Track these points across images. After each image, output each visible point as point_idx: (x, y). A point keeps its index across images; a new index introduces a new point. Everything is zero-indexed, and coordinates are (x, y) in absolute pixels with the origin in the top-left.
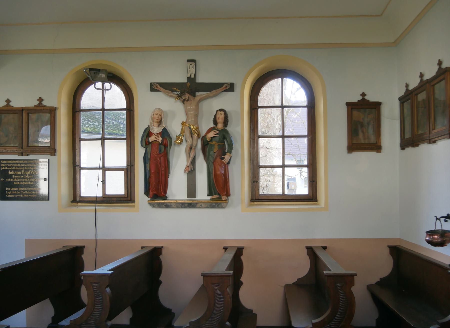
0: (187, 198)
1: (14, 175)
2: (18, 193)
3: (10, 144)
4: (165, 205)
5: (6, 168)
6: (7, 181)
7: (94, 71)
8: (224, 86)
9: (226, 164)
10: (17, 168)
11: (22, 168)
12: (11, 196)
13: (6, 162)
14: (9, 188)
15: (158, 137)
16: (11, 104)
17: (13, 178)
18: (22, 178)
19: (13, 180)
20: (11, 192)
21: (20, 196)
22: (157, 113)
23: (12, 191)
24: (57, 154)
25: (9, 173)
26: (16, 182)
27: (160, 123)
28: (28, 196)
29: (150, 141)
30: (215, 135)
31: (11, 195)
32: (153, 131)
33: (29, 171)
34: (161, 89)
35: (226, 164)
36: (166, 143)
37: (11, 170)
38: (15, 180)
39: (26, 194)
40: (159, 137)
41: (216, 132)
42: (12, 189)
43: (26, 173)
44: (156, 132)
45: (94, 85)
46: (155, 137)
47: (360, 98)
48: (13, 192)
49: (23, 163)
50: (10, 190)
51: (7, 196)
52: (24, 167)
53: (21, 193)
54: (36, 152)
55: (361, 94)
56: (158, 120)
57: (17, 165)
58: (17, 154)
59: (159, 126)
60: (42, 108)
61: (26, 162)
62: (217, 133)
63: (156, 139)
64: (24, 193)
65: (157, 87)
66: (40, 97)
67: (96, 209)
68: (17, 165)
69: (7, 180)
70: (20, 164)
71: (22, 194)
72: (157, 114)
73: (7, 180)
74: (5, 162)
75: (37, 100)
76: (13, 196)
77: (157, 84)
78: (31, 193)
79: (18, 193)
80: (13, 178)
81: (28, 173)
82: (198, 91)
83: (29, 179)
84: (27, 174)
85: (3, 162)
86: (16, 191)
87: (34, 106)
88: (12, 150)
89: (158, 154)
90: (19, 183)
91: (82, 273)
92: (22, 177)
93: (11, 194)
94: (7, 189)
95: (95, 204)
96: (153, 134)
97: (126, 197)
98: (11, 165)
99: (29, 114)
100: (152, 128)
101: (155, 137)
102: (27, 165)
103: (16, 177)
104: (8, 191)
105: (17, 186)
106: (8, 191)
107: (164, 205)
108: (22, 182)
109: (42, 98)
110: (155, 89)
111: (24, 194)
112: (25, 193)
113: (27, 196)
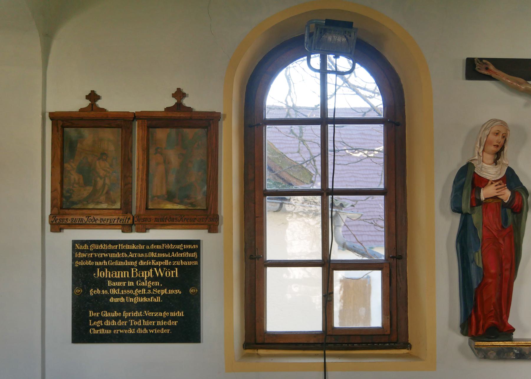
1: (110, 279)
2: (120, 323)
3: (98, 203)
4: (514, 353)
5: (90, 263)
6: (91, 294)
10: (117, 263)
11: (131, 263)
12: (102, 331)
13: (89, 248)
14: (96, 312)
16: (100, 104)
17: (108, 288)
18: (131, 288)
19: (109, 292)
20: (103, 323)
21: (126, 331)
22: (497, 132)
23: (104, 319)
24: (222, 227)
25: (96, 275)
26: (115, 296)
27: (498, 155)
28: (148, 331)
29: (483, 198)
31: (103, 330)
32: (484, 173)
33: (151, 270)
34: (500, 74)
36: (520, 203)
37: (102, 268)
38: (114, 291)
39: (142, 327)
40: (505, 189)
42: (106, 314)
43: (141, 275)
44: (493, 177)
45: (306, 58)
46: (497, 189)
47: (172, 102)
48: (108, 323)
49: (134, 251)
50: (101, 318)
51: (92, 331)
52: (139, 259)
53: (129, 324)
54: (171, 222)
55: (87, 94)
57: (118, 255)
59: (495, 162)
60: (182, 115)
61: (141, 247)
64: (136, 323)
65: (487, 69)
66: (91, 91)
67: (325, 362)
68: (118, 255)
69: (92, 292)
70: (128, 251)
71: (133, 327)
72: (497, 134)
73: (92, 292)
74: (86, 247)
75: (171, 96)
76: (109, 332)
77: (488, 63)
78: (156, 323)
79: (120, 323)
80: (108, 288)
81: (147, 273)
83: (151, 289)
84: (146, 276)
85: (81, 248)
86: (116, 319)
87: (164, 110)
88: (107, 218)
89: (500, 228)
90: (122, 300)
92: (130, 284)
93: (101, 327)
94: (91, 314)
95: (322, 352)
96: (490, 182)
97: (387, 335)
98: (101, 255)
99: (65, 129)
100: (480, 166)
101: (497, 189)
102: (146, 255)
103: (114, 284)
104: (94, 319)
105: (120, 307)
106: (94, 319)
107: (512, 353)
108: (133, 296)
109: (96, 92)
110: (481, 73)
111: (137, 327)
112: (139, 323)
113: (145, 331)
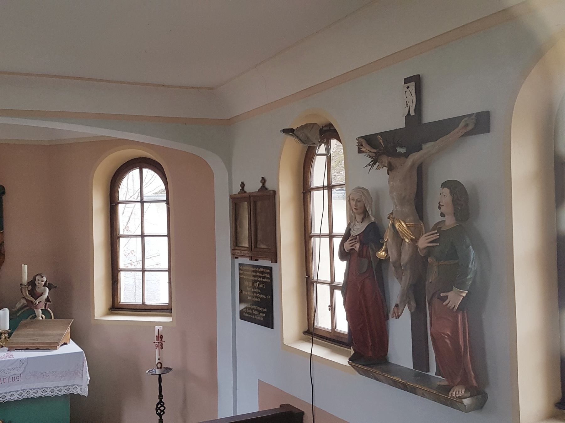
0: (435, 375)
7: (13, 359)
8: (462, 124)
9: (455, 310)
15: (354, 243)
30: (430, 242)
35: (455, 310)
41: (434, 235)
46: (350, 244)
56: (358, 210)
58: (248, 257)
62: (435, 240)
63: (352, 246)
82: (405, 153)
91: (47, 289)
101: (350, 244)
